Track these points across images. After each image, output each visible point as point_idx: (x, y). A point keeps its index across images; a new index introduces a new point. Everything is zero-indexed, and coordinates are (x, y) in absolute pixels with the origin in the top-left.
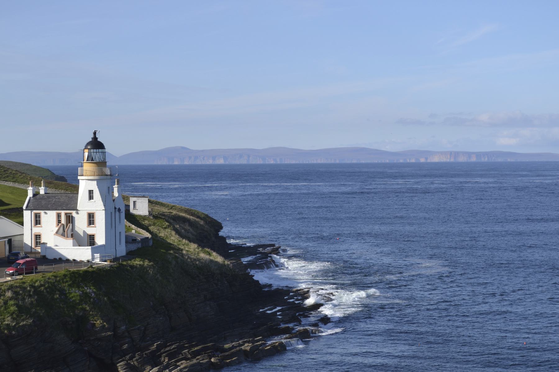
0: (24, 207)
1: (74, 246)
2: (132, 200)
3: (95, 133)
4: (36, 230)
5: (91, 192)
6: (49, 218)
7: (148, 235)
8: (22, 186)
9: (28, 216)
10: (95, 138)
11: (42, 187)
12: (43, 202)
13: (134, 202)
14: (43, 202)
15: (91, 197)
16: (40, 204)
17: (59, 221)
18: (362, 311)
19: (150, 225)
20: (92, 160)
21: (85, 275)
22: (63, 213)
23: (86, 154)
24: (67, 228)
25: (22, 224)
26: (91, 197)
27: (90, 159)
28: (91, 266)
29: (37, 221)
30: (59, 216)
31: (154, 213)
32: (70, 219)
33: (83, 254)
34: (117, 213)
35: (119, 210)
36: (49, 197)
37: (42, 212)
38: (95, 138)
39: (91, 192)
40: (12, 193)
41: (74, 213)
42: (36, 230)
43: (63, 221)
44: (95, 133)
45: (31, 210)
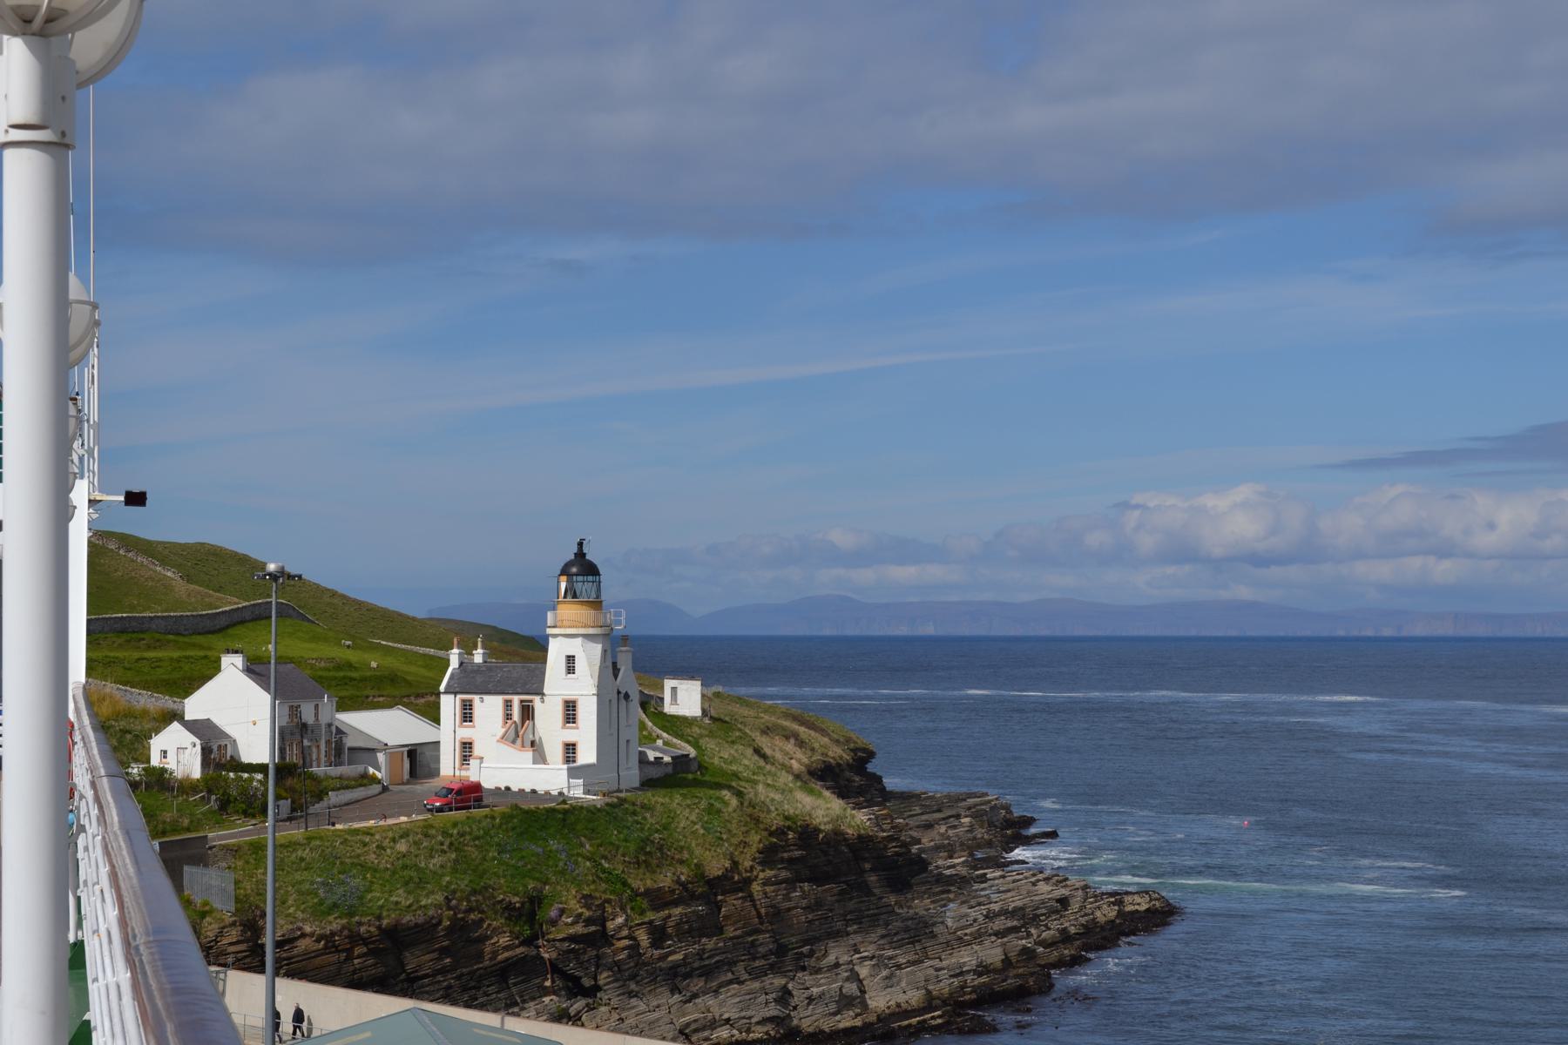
0: (442, 688)
1: (534, 762)
2: (669, 684)
3: (580, 544)
4: (465, 733)
5: (570, 659)
6: (489, 708)
7: (692, 753)
8: (441, 653)
9: (449, 705)
10: (580, 555)
11: (480, 651)
12: (479, 679)
13: (674, 690)
14: (479, 679)
15: (570, 669)
16: (472, 683)
17: (508, 716)
18: (427, 826)
19: (701, 736)
20: (575, 596)
21: (534, 818)
22: (516, 699)
23: (563, 586)
24: (521, 726)
25: (436, 720)
26: (570, 669)
27: (572, 593)
28: (564, 802)
29: (467, 715)
30: (508, 705)
31: (713, 713)
32: (527, 712)
33: (551, 779)
34: (623, 702)
35: (627, 696)
36: (490, 669)
37: (476, 698)
38: (580, 555)
39: (570, 659)
40: (426, 667)
41: (537, 699)
42: (465, 733)
43: (516, 716)
44: (580, 544)
45: (455, 694)
